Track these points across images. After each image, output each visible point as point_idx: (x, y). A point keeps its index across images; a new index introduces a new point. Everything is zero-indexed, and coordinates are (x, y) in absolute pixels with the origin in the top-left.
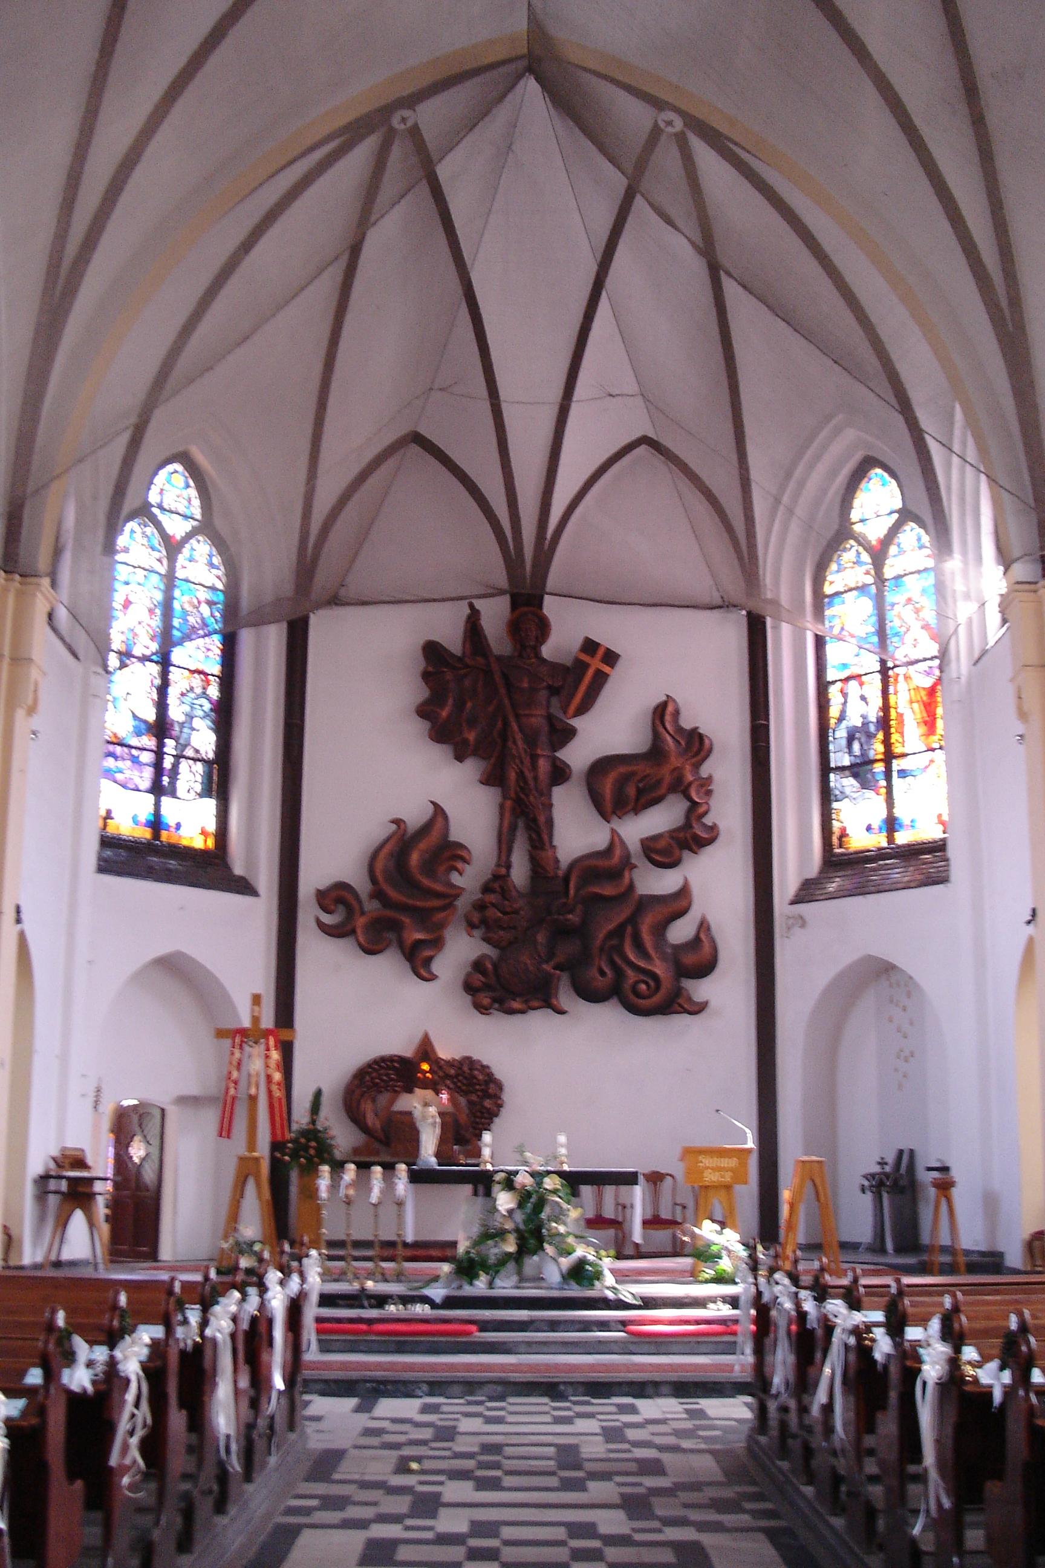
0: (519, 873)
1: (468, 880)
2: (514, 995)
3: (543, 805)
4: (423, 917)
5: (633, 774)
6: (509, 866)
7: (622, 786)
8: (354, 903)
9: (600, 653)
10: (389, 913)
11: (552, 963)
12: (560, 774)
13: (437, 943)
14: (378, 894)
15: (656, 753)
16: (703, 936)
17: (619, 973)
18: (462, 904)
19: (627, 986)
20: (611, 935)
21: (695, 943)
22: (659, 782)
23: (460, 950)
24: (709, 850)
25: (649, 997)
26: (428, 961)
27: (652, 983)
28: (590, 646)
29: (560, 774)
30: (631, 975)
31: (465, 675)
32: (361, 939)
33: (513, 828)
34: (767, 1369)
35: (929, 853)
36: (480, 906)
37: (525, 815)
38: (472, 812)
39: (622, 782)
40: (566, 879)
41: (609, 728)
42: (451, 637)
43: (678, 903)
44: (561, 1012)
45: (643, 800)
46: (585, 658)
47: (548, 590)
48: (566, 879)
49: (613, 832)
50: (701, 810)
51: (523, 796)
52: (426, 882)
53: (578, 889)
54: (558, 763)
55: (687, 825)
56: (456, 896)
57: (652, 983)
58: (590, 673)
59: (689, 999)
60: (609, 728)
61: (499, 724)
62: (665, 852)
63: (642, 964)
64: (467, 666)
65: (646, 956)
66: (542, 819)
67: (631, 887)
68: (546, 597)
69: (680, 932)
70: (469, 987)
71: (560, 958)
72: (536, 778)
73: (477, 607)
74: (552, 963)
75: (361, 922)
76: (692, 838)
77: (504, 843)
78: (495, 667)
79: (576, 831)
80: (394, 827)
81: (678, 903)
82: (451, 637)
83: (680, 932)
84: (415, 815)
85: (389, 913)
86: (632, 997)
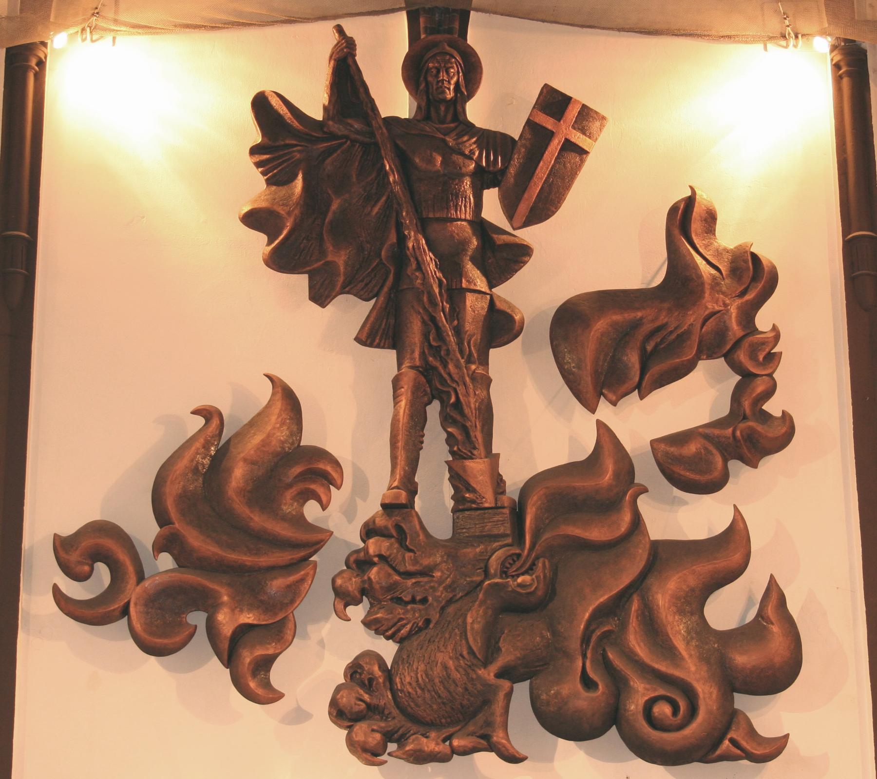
0: (435, 505)
1: (343, 517)
2: (426, 725)
3: (473, 378)
4: (248, 583)
5: (636, 325)
6: (413, 491)
7: (616, 344)
8: (123, 557)
9: (572, 112)
10: (191, 577)
11: (494, 668)
12: (501, 326)
13: (278, 631)
14: (167, 543)
15: (680, 282)
16: (770, 612)
17: (619, 686)
18: (329, 563)
19: (634, 706)
20: (602, 613)
21: (752, 632)
22: (683, 338)
23: (329, 645)
24: (771, 463)
25: (680, 727)
26: (265, 664)
27: (683, 705)
28: (554, 102)
29: (501, 326)
30: (640, 691)
31: (329, 152)
32: (138, 626)
33: (418, 420)
34: (506, 753)
35: (393, 696)
36: (359, 563)
37: (443, 391)
38: (343, 388)
39: (623, 336)
40: (518, 512)
41: (592, 245)
42: (312, 98)
43: (729, 551)
44: (513, 758)
45: (655, 369)
46: (548, 122)
47: (473, 6)
48: (518, 512)
49: (602, 428)
50: (760, 387)
51: (437, 364)
52: (258, 520)
53: (536, 535)
54: (499, 305)
55: (736, 414)
56: (316, 546)
57: (683, 705)
58: (555, 145)
59: (752, 732)
60: (592, 245)
61: (393, 238)
62: (694, 463)
63: (662, 667)
64: (333, 136)
65: (668, 650)
66: (471, 403)
67: (637, 522)
68: (472, 13)
69: (727, 609)
70: (340, 713)
71: (507, 656)
72: (458, 331)
73: (349, 33)
74: (494, 668)
75: (134, 593)
76: (751, 434)
77: (407, 446)
78: (381, 136)
79: (538, 426)
80: (200, 421)
81: (729, 551)
82: (312, 98)
83: (727, 609)
84: (241, 395)
85: (191, 577)
86: (655, 735)
